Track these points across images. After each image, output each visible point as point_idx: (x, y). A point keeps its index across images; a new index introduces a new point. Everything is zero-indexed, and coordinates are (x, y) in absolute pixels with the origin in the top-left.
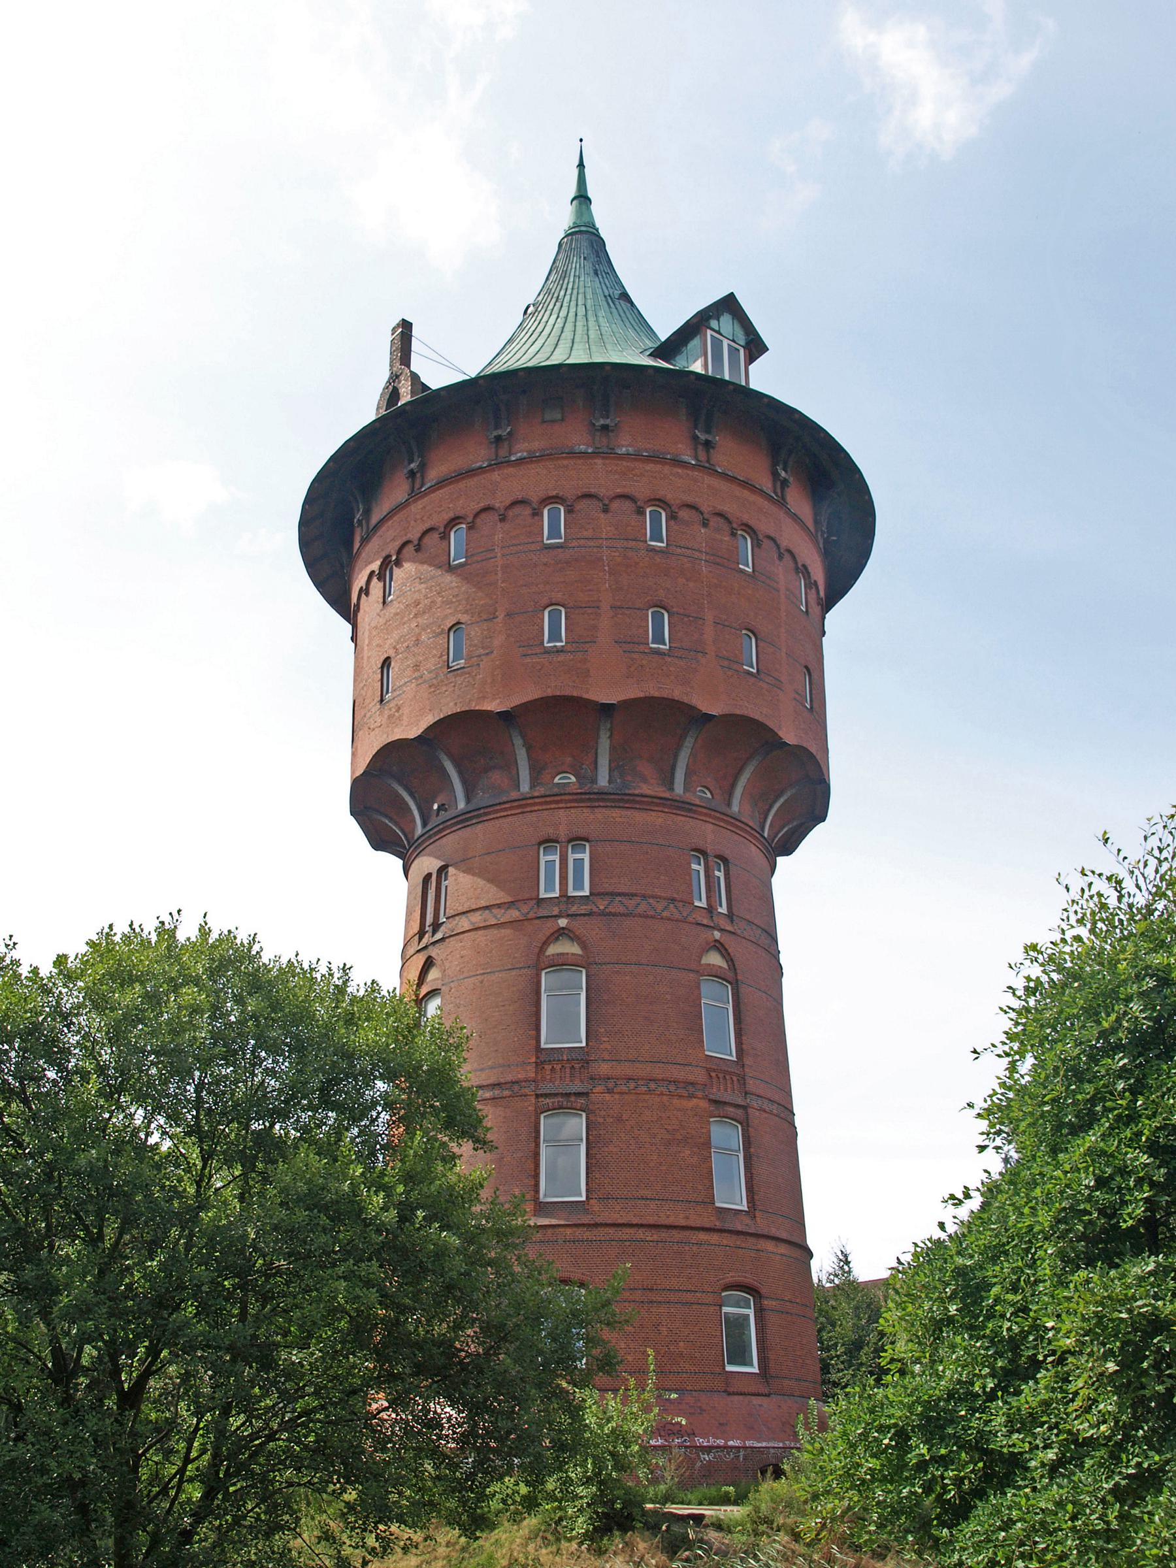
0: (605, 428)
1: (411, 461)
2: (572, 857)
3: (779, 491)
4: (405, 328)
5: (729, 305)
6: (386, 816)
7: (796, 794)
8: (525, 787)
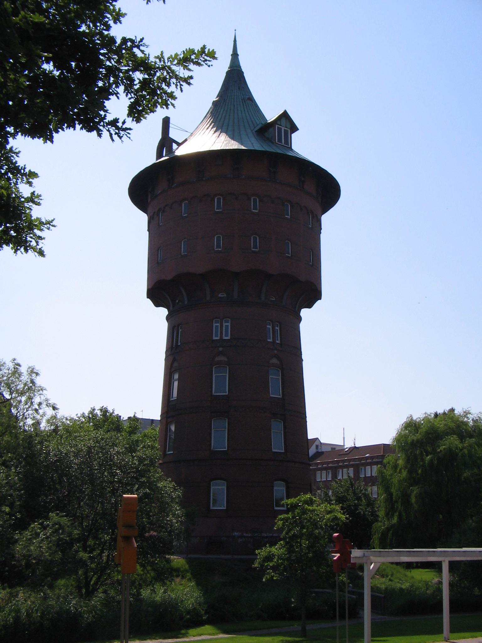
2: (224, 324)
7: (311, 294)
8: (208, 298)
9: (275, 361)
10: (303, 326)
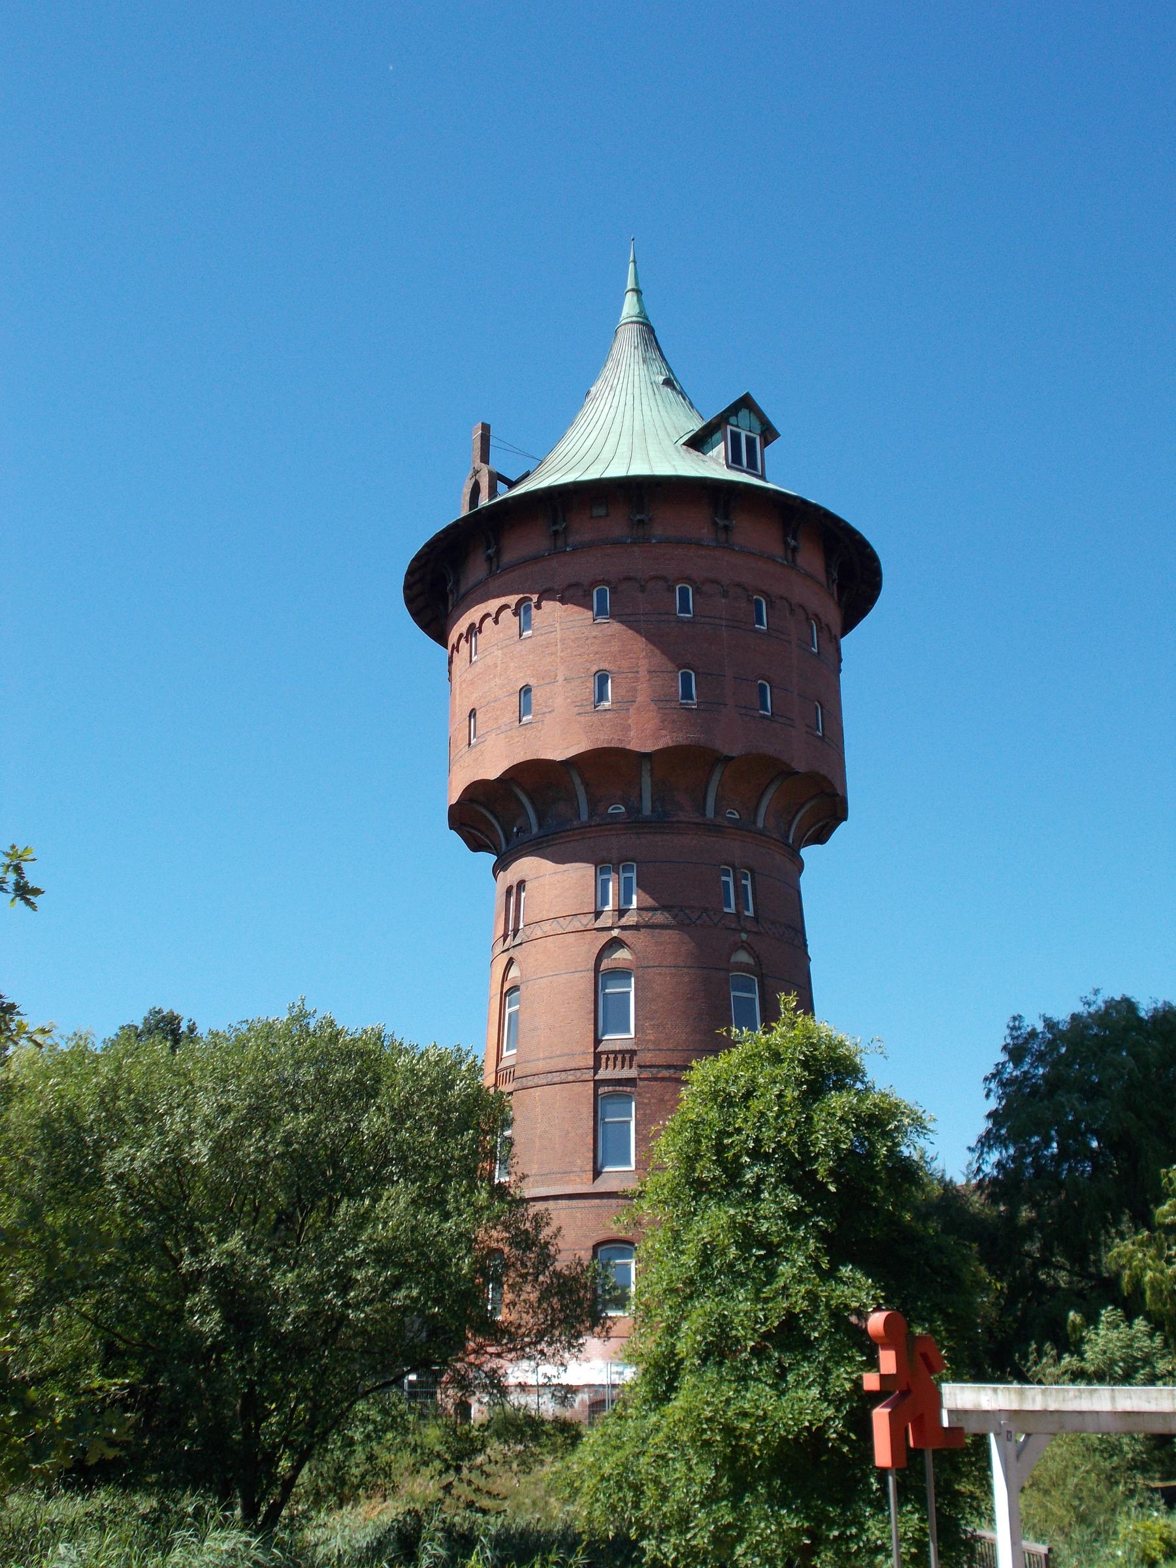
0: (641, 522)
1: (488, 548)
3: (790, 558)
4: (486, 428)
5: (746, 403)
6: (479, 831)
7: (825, 809)
8: (584, 817)
9: (742, 957)
10: (806, 881)
